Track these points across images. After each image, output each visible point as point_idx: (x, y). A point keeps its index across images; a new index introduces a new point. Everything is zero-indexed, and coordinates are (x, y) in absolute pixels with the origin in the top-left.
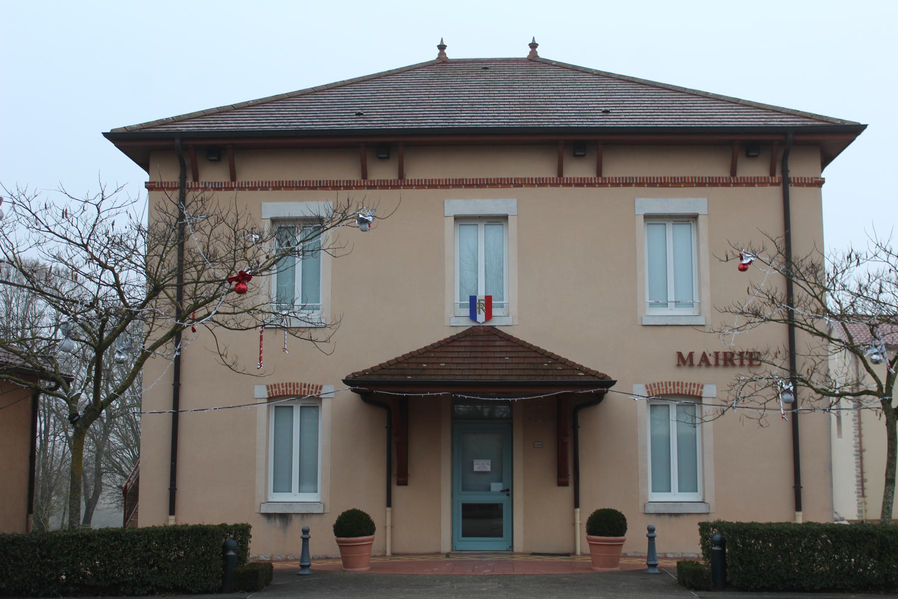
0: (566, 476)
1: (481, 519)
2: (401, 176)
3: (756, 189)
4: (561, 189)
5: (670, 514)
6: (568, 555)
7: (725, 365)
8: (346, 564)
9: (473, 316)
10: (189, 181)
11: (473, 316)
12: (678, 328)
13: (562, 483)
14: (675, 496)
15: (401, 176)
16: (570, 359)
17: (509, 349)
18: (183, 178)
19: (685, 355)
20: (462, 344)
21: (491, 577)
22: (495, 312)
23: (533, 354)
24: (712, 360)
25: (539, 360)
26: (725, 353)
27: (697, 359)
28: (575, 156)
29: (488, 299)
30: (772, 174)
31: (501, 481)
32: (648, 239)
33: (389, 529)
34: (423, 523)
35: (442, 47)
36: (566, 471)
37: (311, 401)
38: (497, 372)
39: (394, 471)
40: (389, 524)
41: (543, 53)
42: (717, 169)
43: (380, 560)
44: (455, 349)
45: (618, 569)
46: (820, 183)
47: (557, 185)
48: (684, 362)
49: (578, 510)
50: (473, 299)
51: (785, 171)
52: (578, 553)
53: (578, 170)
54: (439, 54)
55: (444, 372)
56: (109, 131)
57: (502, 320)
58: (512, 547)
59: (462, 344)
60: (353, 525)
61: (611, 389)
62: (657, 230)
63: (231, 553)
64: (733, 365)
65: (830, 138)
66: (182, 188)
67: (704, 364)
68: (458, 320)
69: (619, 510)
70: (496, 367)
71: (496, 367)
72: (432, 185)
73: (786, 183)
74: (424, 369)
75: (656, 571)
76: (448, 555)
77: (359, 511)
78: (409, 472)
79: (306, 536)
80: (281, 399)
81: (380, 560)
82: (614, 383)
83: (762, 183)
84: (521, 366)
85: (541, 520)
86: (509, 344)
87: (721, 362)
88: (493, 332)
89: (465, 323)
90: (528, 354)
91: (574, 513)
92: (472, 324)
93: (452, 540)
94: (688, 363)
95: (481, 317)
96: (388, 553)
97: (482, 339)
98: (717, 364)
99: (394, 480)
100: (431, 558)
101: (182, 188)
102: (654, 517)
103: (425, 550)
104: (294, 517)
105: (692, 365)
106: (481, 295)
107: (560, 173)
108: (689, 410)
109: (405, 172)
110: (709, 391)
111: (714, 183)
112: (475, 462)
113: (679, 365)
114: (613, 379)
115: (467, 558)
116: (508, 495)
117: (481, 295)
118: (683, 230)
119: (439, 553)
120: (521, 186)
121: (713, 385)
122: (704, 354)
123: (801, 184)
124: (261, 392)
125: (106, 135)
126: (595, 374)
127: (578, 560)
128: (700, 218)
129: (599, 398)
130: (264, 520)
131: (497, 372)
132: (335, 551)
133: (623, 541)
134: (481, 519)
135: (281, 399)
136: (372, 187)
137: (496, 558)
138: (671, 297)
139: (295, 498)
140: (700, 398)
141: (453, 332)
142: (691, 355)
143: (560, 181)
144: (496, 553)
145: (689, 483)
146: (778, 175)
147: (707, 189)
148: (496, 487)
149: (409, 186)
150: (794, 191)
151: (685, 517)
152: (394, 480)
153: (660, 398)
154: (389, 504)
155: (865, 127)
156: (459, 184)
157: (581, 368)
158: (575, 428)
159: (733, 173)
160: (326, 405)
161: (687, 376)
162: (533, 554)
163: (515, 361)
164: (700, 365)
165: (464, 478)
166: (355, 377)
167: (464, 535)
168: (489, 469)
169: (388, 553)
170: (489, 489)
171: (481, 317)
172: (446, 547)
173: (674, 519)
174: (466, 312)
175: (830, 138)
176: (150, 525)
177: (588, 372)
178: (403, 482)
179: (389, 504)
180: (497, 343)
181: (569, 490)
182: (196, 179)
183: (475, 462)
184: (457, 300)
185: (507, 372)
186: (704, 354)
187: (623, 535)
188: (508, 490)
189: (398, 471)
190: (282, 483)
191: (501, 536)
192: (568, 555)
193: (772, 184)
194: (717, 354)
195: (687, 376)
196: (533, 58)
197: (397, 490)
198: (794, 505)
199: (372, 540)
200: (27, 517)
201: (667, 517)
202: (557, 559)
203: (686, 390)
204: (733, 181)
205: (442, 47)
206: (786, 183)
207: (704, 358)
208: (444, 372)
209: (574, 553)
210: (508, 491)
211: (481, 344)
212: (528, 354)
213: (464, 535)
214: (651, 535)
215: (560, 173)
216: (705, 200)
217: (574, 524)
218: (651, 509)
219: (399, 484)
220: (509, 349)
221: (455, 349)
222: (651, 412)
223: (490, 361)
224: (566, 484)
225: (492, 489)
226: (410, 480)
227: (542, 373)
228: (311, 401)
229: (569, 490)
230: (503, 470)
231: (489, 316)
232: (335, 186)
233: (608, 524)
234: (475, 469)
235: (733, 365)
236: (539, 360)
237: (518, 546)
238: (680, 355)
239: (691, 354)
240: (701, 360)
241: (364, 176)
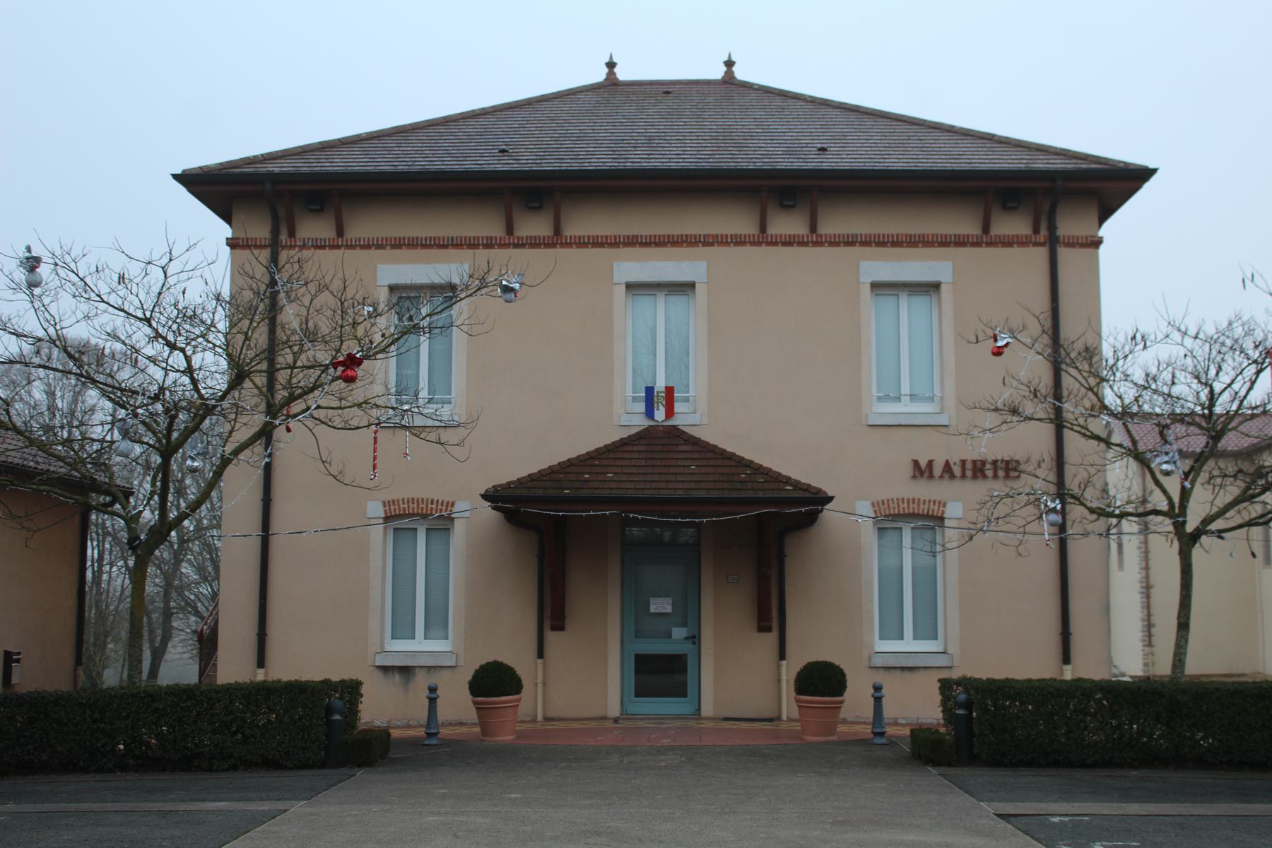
0: (769, 619)
1: (661, 674)
2: (557, 231)
3: (1016, 251)
4: (764, 249)
5: (903, 669)
6: (771, 720)
7: (975, 477)
8: (485, 730)
9: (650, 413)
10: (284, 237)
11: (650, 413)
12: (914, 431)
13: (763, 627)
14: (909, 644)
15: (557, 231)
16: (774, 469)
17: (696, 455)
18: (275, 232)
19: (923, 464)
20: (635, 448)
21: (672, 748)
22: (678, 407)
23: (726, 462)
24: (957, 470)
25: (734, 470)
26: (974, 462)
27: (938, 470)
28: (784, 207)
29: (670, 391)
30: (1036, 230)
31: (685, 625)
32: (874, 312)
33: (540, 687)
34: (585, 677)
35: (611, 65)
36: (769, 613)
37: (440, 522)
38: (680, 485)
39: (548, 613)
40: (540, 680)
41: (740, 73)
42: (968, 226)
43: (529, 726)
44: (626, 455)
45: (834, 738)
46: (1097, 243)
47: (758, 243)
48: (922, 473)
49: (784, 663)
50: (650, 391)
51: (1052, 228)
52: (784, 717)
53: (787, 224)
54: (608, 74)
55: (613, 485)
56: (179, 172)
57: (688, 417)
58: (699, 710)
59: (635, 448)
60: (494, 681)
61: (828, 506)
62: (887, 302)
63: (337, 717)
64: (985, 477)
65: (1111, 184)
66: (275, 246)
67: (946, 476)
68: (631, 418)
69: (837, 663)
70: (679, 478)
71: (679, 478)
72: (598, 243)
73: (1053, 243)
74: (587, 481)
75: (884, 741)
76: (616, 720)
77: (501, 664)
78: (567, 613)
79: (433, 696)
80: (401, 519)
81: (529, 726)
82: (830, 499)
83: (1023, 242)
84: (711, 478)
85: (736, 675)
86: (696, 448)
87: (969, 473)
88: (675, 434)
89: (641, 422)
90: (720, 462)
91: (779, 667)
92: (647, 423)
93: (622, 701)
94: (927, 474)
95: (660, 414)
96: (540, 718)
97: (662, 443)
98: (963, 476)
99: (547, 624)
100: (594, 724)
101: (275, 246)
102: (882, 671)
103: (586, 715)
104: (417, 670)
105: (931, 476)
106: (660, 385)
107: (763, 229)
108: (928, 535)
109: (562, 225)
110: (954, 511)
111: (960, 242)
112: (652, 600)
113: (914, 477)
114: (830, 494)
115: (641, 724)
116: (694, 643)
117: (660, 385)
118: (921, 302)
119: (604, 718)
120: (712, 244)
121: (958, 504)
122: (947, 463)
123: (1072, 243)
124: (376, 510)
125: (175, 177)
126: (807, 488)
127: (784, 726)
128: (943, 287)
129: (811, 518)
130: (379, 675)
131: (680, 485)
132: (471, 714)
133: (842, 702)
134: (661, 674)
135: (401, 519)
136: (519, 245)
137: (679, 723)
138: (905, 389)
139: (420, 646)
140: (942, 519)
141: (625, 434)
142: (930, 463)
143: (763, 238)
144: (678, 717)
145: (926, 629)
146: (1044, 232)
147: (952, 251)
148: (679, 633)
149: (568, 245)
150: (1064, 253)
151: (922, 672)
152: (547, 624)
153: (890, 519)
154: (541, 654)
155: (1154, 171)
156: (631, 242)
157: (788, 480)
158: (781, 557)
159: (986, 229)
160: (459, 528)
161: (925, 491)
162: (726, 719)
163: (703, 470)
164: (941, 477)
165: (637, 620)
166: (496, 491)
167: (638, 694)
168: (669, 609)
169: (540, 718)
170: (670, 636)
171: (660, 414)
172: (614, 710)
173: (907, 675)
174: (641, 407)
175: (1111, 184)
176: (318, 677)
177: (797, 485)
178: (559, 626)
179: (541, 654)
180: (680, 448)
181: (772, 637)
182: (292, 234)
183: (652, 600)
184: (629, 393)
185: (693, 485)
186: (947, 463)
187: (841, 695)
188: (694, 637)
189: (552, 612)
190: (403, 628)
191: (684, 695)
192: (771, 720)
193: (1036, 244)
194: (963, 462)
195: (925, 491)
196: (729, 79)
197: (551, 637)
198: (1060, 657)
199: (519, 700)
200: (75, 670)
201: (898, 672)
202: (757, 725)
203: (923, 509)
204: (985, 239)
205: (611, 65)
206: (1053, 243)
207: (947, 468)
208: (613, 485)
209: (779, 718)
210: (695, 639)
211: (659, 448)
212: (720, 462)
213: (638, 694)
214: (877, 695)
215: (763, 229)
216: (949, 264)
217: (779, 681)
218: (878, 661)
219: (554, 628)
220: (696, 455)
221: (626, 455)
222: (880, 537)
223: (672, 470)
224: (769, 630)
225: (674, 636)
226: (569, 624)
227: (738, 486)
228: (440, 522)
229: (771, 638)
230: (688, 613)
231: (670, 413)
232: (472, 244)
233: (822, 681)
234: (653, 609)
235: (985, 477)
236: (734, 470)
237: (707, 709)
238: (916, 463)
239: (930, 463)
240: (944, 471)
241: (510, 231)
